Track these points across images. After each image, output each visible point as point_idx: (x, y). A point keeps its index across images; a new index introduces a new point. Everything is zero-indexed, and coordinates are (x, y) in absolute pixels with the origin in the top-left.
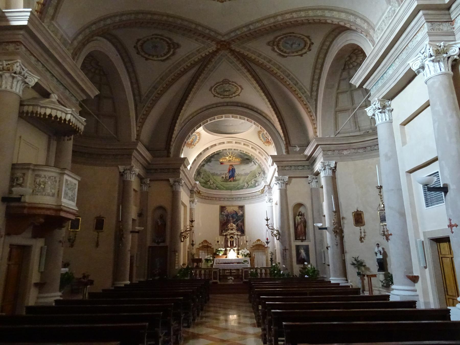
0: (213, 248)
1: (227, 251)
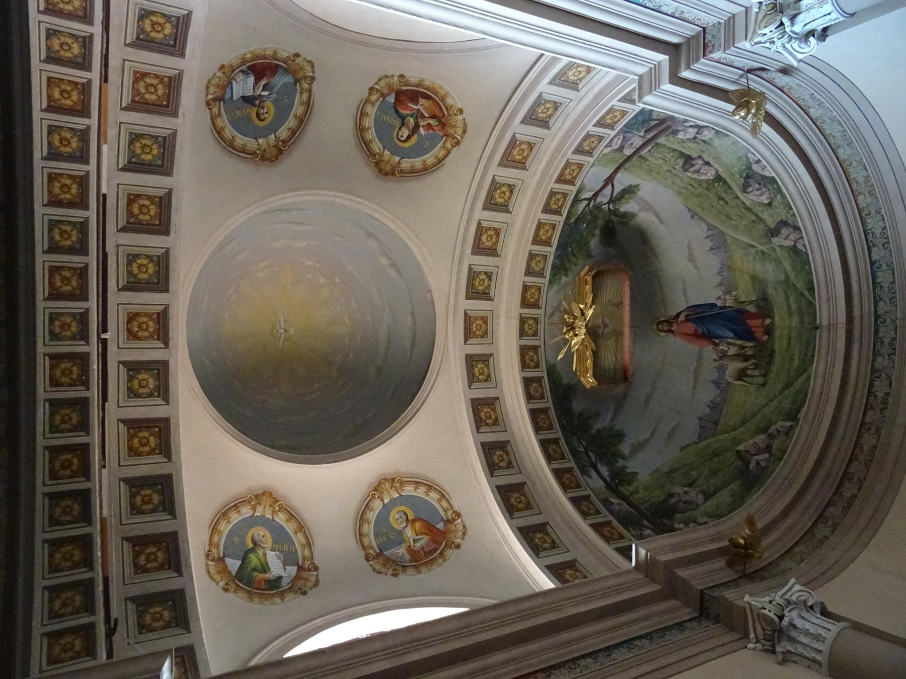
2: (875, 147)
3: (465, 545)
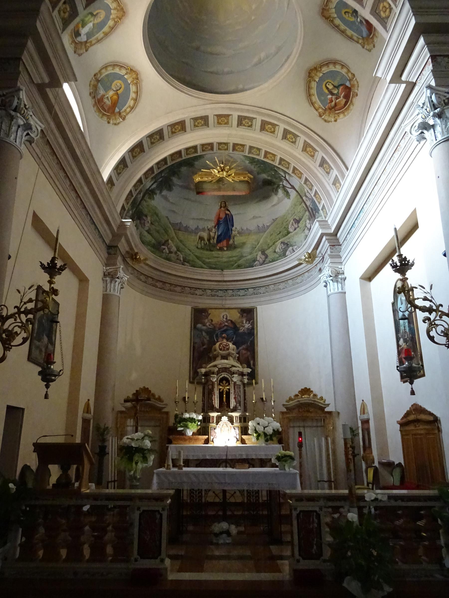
0: (167, 413)
1: (209, 422)
2: (290, 293)
3: (111, 126)
